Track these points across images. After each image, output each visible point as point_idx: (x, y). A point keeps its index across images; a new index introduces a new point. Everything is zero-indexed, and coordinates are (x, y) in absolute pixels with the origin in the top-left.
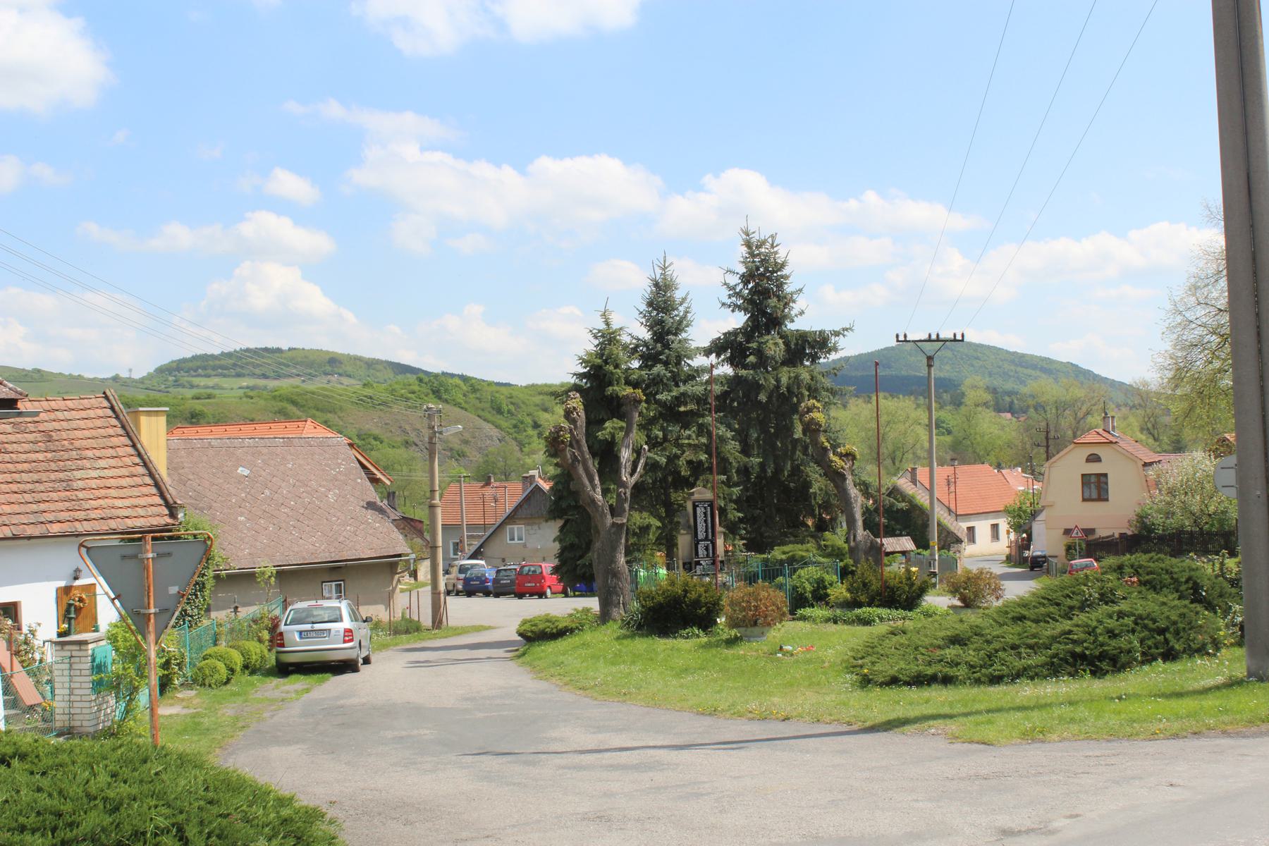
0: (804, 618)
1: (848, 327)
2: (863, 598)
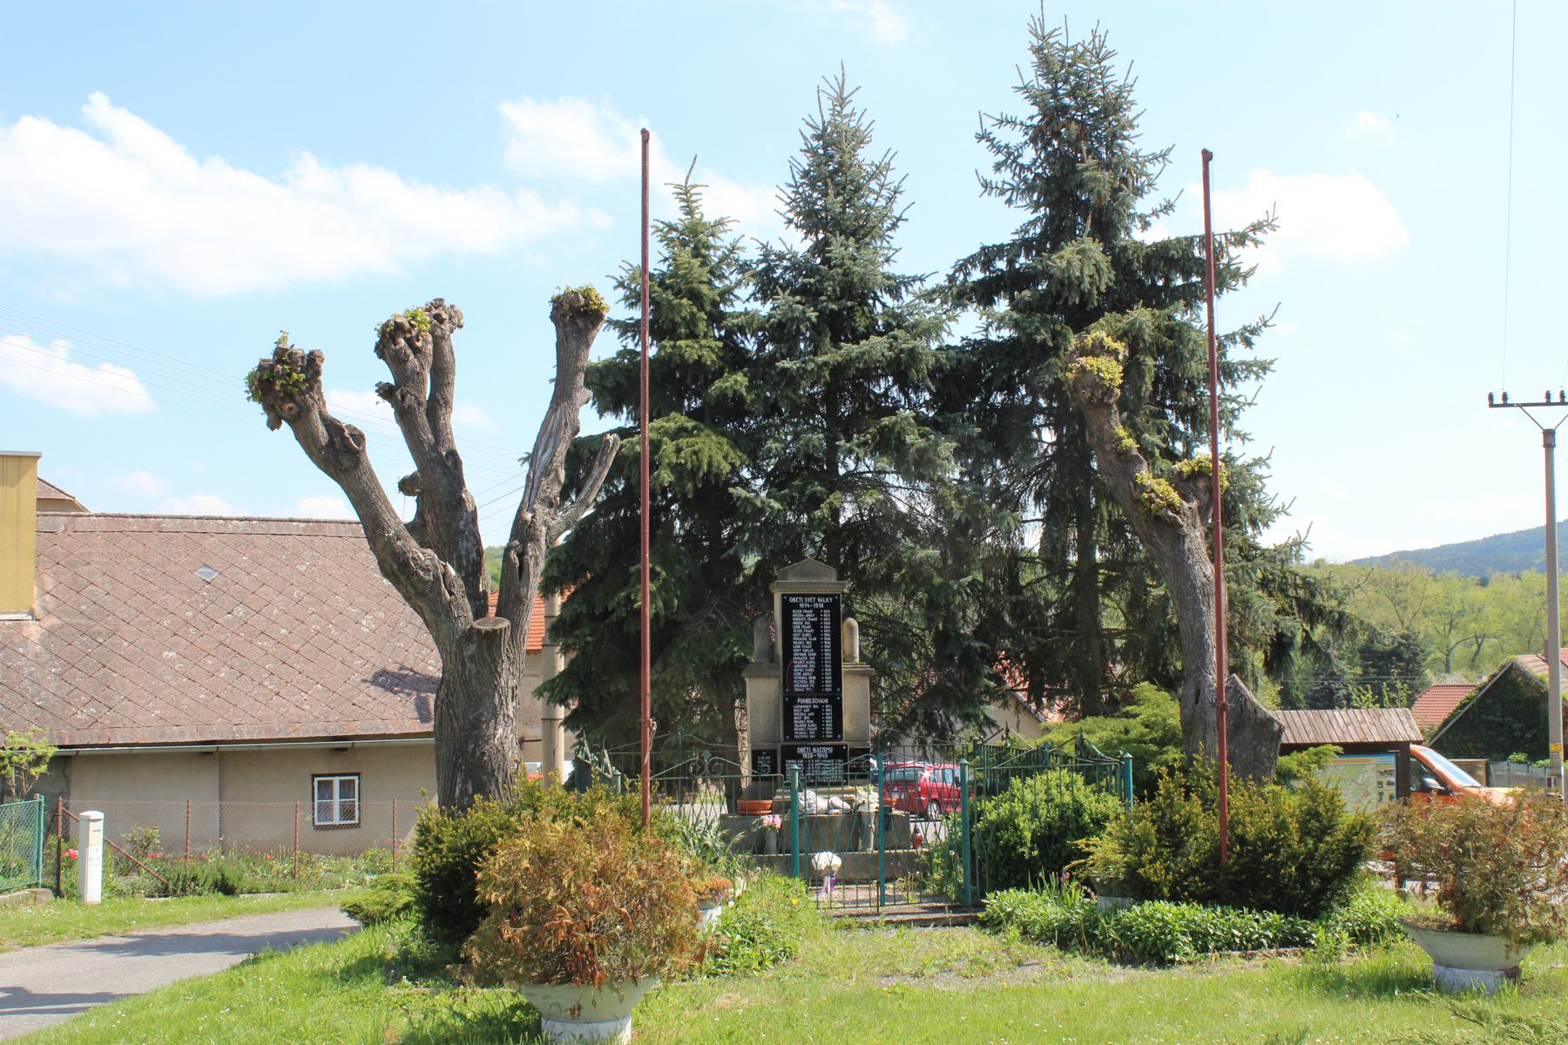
0: (993, 925)
1: (1262, 217)
2: (1154, 871)
